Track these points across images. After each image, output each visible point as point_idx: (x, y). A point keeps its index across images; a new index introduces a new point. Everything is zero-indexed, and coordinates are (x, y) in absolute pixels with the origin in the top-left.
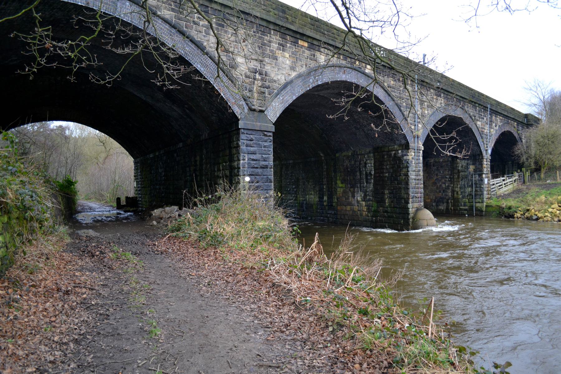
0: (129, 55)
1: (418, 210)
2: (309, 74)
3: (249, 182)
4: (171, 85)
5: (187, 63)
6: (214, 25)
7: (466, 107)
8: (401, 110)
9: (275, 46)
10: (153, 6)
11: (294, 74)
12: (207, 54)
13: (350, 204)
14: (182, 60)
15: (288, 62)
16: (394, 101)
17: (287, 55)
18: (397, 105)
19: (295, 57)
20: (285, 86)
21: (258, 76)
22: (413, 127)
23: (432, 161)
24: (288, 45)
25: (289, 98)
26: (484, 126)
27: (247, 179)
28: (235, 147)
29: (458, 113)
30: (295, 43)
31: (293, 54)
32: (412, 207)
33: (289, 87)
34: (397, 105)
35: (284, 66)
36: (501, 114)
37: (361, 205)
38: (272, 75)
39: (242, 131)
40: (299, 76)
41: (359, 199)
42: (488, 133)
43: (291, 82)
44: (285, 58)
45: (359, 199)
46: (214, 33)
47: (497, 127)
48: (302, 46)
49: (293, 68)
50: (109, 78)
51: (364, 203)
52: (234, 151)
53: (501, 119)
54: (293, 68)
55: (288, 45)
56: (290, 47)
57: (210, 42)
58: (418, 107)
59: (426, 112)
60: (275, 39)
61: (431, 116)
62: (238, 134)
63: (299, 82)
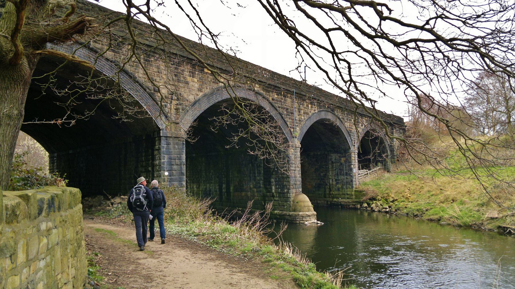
0: (100, 100)
1: (297, 195)
2: (212, 94)
3: (168, 176)
4: (126, 118)
5: (141, 107)
6: (142, 61)
7: (336, 112)
8: (282, 117)
9: (186, 73)
10: (99, 49)
11: (201, 94)
12: (138, 82)
13: (230, 143)
14: (137, 104)
15: (196, 85)
16: (277, 110)
17: (196, 80)
18: (279, 113)
19: (202, 82)
20: (195, 103)
21: (175, 97)
22: (292, 130)
23: (312, 154)
24: (197, 73)
25: (197, 112)
26: (352, 126)
27: (166, 173)
28: (157, 150)
29: (330, 116)
30: (202, 71)
31: (200, 79)
32: (292, 194)
33: (197, 104)
34: (279, 113)
35: (193, 88)
36: (365, 116)
37: (253, 191)
38: (185, 96)
39: (163, 138)
40: (205, 95)
41: (251, 186)
42: (354, 131)
43: (199, 100)
44: (194, 83)
45: (251, 186)
46: (142, 66)
47: (363, 126)
48: (207, 73)
49: (200, 90)
50: (87, 114)
51: (255, 190)
52: (156, 152)
53: (366, 120)
54: (200, 90)
55: (197, 73)
56: (198, 74)
57: (140, 75)
58: (296, 114)
59: (303, 118)
60: (186, 69)
61: (307, 120)
62: (160, 140)
63: (205, 100)
